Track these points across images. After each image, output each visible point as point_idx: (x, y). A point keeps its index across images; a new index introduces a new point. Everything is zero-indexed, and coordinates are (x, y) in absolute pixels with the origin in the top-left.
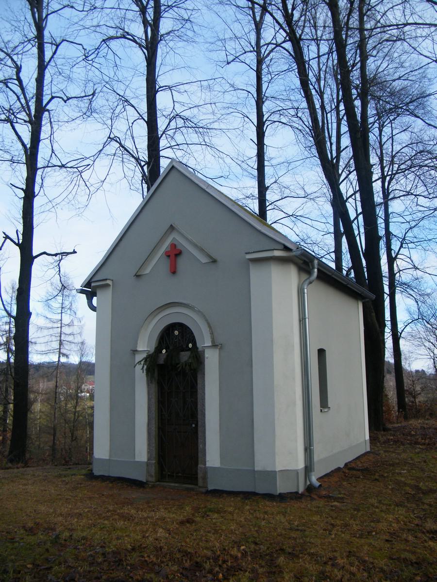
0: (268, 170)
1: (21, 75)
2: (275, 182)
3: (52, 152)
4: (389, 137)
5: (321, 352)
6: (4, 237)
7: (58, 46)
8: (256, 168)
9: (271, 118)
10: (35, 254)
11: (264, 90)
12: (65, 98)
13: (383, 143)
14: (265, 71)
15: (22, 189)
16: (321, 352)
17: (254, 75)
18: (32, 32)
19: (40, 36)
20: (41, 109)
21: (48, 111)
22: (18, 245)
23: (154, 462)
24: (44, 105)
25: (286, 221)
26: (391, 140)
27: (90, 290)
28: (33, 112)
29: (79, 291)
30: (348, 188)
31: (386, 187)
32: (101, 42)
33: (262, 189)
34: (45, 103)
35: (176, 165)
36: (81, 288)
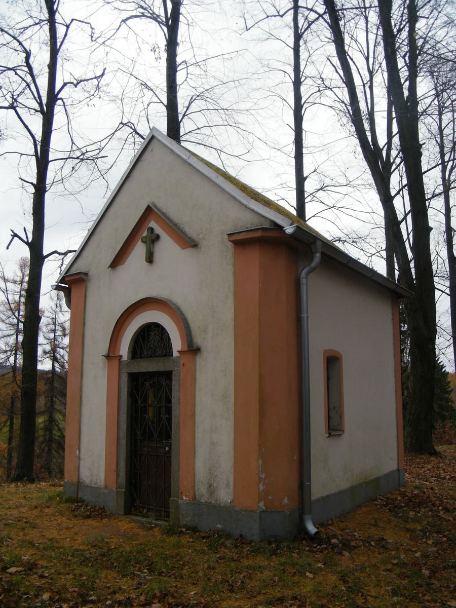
0: (307, 160)
1: (31, 61)
2: (315, 171)
3: (72, 143)
4: (450, 121)
5: (332, 361)
6: (12, 235)
7: (68, 27)
8: (294, 156)
9: (311, 100)
10: (45, 253)
11: (302, 69)
12: (75, 82)
13: (443, 128)
14: (302, 49)
15: (32, 183)
16: (332, 361)
17: (291, 52)
18: (45, 15)
19: (52, 22)
20: (53, 97)
21: (61, 99)
22: (27, 243)
23: (124, 490)
24: (56, 91)
25: (328, 214)
26: (452, 123)
27: (67, 286)
28: (44, 101)
29: (55, 287)
30: (311, 104)
31: (447, 178)
32: (121, 23)
33: (301, 180)
34: (57, 90)
35: (156, 135)
36: (57, 284)
